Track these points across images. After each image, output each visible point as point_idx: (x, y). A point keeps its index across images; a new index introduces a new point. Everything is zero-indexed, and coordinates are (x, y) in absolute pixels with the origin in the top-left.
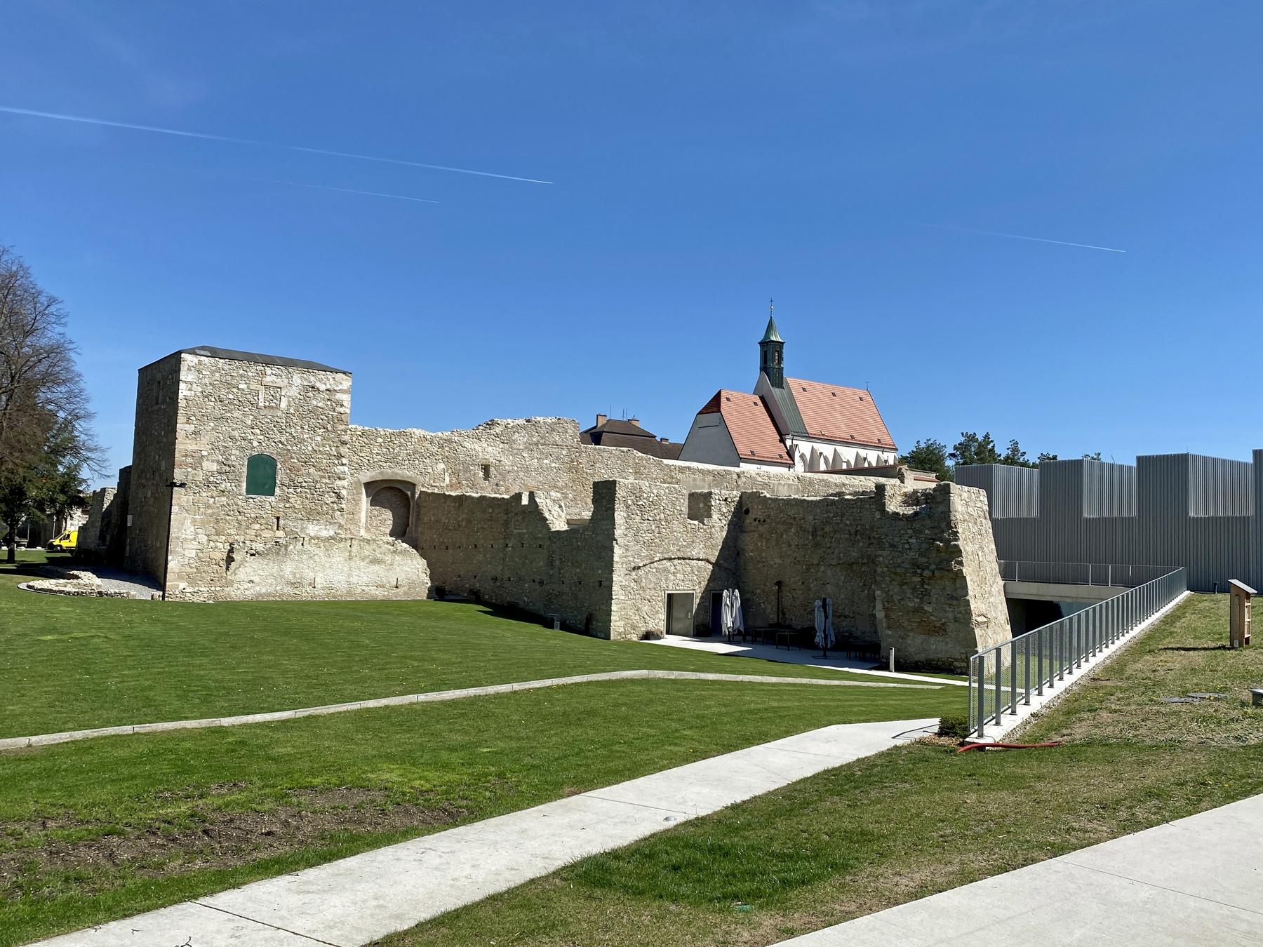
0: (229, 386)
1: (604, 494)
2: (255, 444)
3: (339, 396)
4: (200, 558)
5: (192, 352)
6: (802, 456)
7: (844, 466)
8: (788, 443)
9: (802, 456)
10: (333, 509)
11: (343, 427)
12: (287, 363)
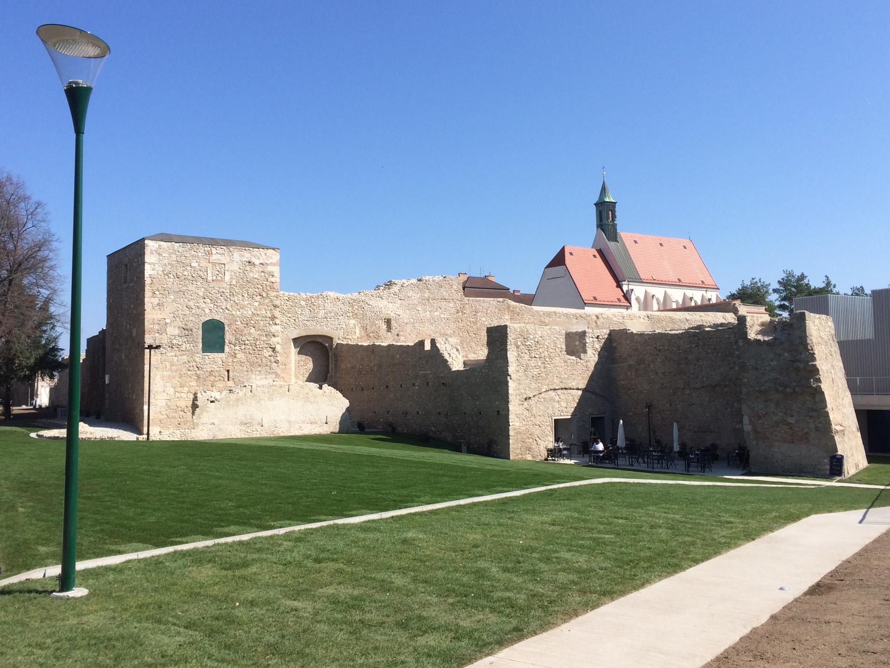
0: (184, 265)
1: (497, 338)
2: (207, 311)
3: (270, 268)
4: (169, 407)
5: (153, 238)
6: (638, 299)
7: (674, 306)
8: (625, 288)
9: (638, 299)
10: (270, 361)
11: (275, 294)
12: (228, 243)
